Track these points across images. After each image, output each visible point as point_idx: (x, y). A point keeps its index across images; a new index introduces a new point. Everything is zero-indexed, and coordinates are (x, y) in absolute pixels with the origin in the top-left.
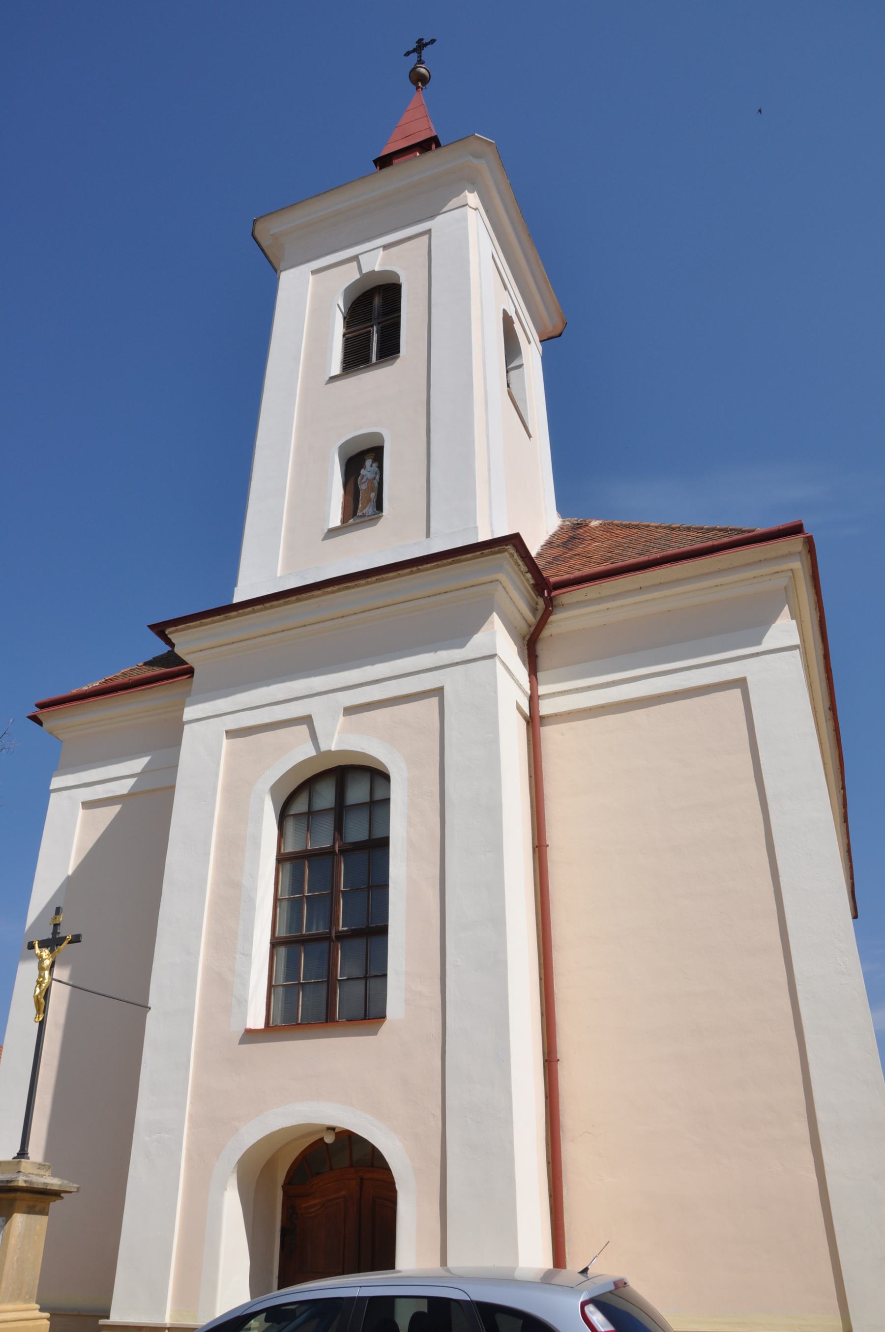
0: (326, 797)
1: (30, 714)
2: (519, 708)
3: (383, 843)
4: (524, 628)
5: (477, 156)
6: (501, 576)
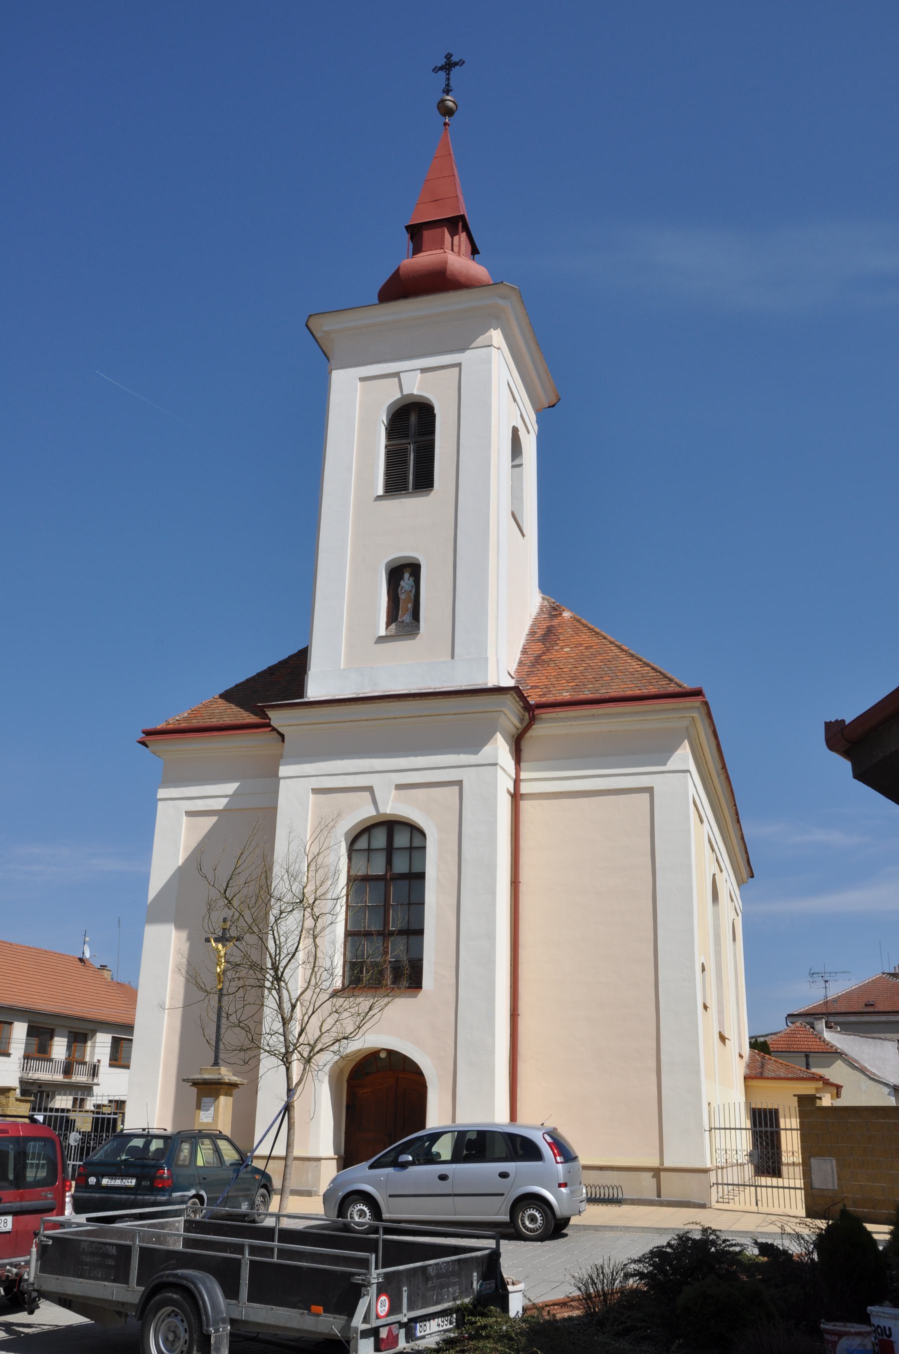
0: (380, 839)
1: (138, 739)
2: (508, 791)
3: (421, 876)
4: (513, 731)
5: (502, 297)
6: (504, 710)
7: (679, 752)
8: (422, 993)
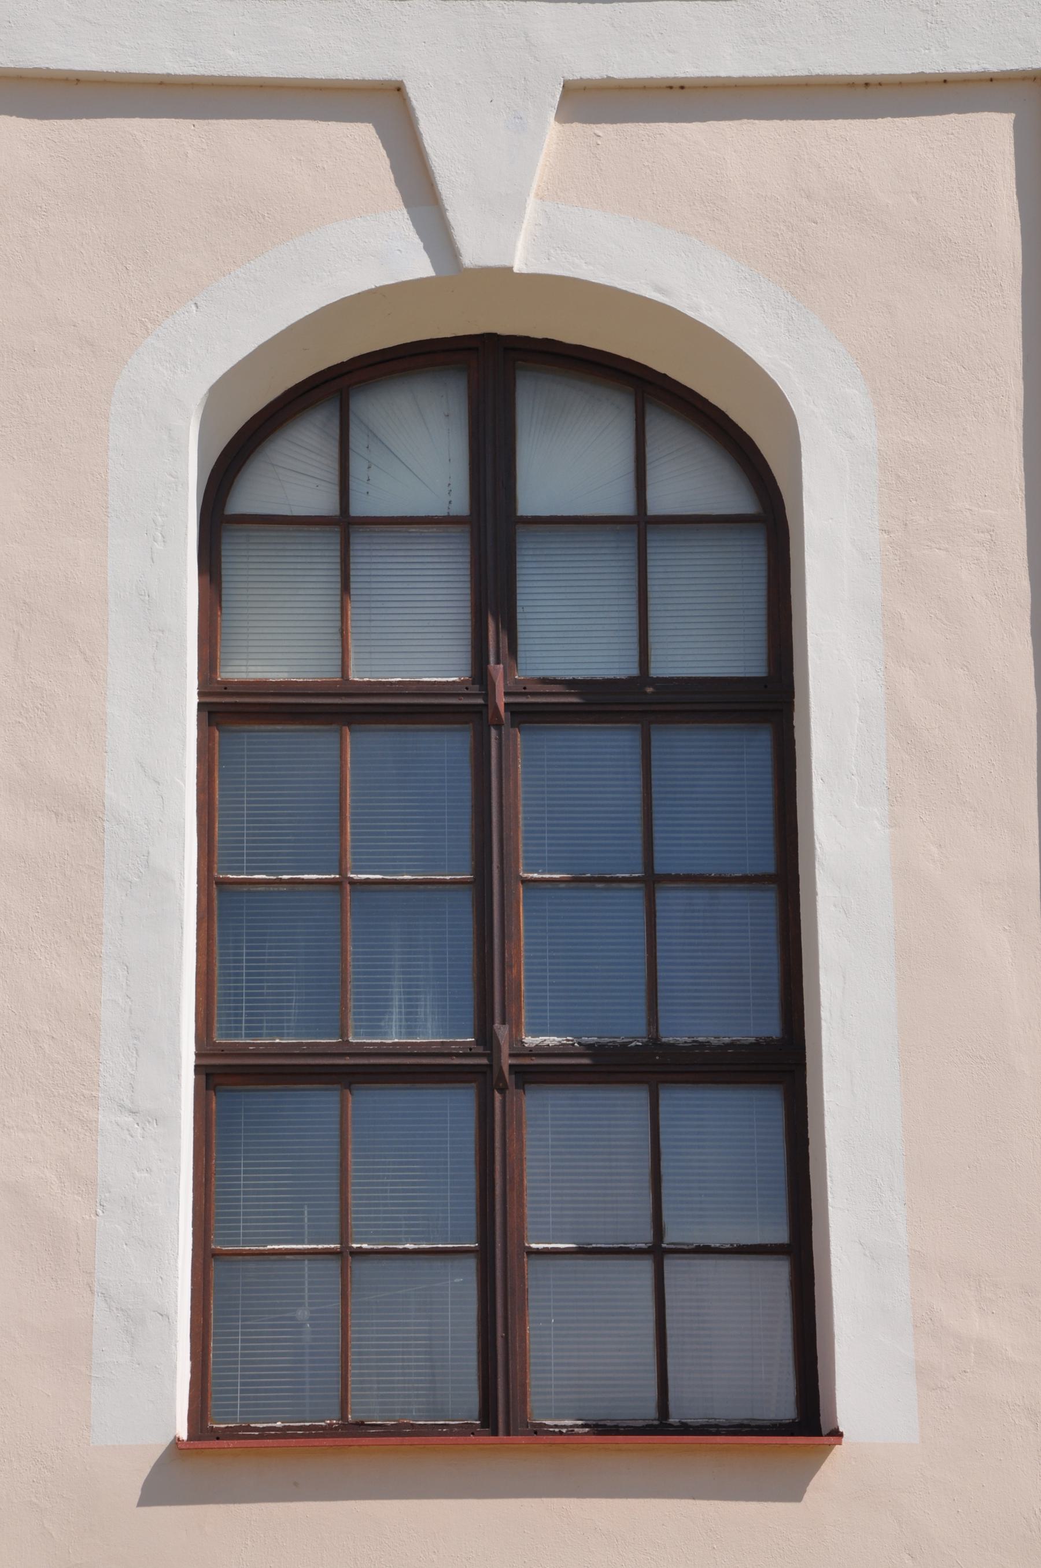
0: (417, 457)
7: (432, 269)
8: (836, 1468)
